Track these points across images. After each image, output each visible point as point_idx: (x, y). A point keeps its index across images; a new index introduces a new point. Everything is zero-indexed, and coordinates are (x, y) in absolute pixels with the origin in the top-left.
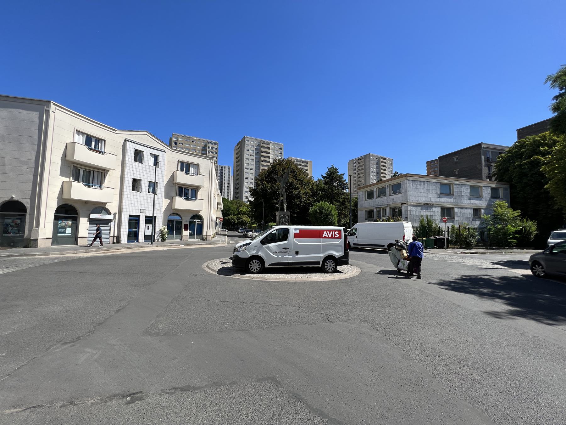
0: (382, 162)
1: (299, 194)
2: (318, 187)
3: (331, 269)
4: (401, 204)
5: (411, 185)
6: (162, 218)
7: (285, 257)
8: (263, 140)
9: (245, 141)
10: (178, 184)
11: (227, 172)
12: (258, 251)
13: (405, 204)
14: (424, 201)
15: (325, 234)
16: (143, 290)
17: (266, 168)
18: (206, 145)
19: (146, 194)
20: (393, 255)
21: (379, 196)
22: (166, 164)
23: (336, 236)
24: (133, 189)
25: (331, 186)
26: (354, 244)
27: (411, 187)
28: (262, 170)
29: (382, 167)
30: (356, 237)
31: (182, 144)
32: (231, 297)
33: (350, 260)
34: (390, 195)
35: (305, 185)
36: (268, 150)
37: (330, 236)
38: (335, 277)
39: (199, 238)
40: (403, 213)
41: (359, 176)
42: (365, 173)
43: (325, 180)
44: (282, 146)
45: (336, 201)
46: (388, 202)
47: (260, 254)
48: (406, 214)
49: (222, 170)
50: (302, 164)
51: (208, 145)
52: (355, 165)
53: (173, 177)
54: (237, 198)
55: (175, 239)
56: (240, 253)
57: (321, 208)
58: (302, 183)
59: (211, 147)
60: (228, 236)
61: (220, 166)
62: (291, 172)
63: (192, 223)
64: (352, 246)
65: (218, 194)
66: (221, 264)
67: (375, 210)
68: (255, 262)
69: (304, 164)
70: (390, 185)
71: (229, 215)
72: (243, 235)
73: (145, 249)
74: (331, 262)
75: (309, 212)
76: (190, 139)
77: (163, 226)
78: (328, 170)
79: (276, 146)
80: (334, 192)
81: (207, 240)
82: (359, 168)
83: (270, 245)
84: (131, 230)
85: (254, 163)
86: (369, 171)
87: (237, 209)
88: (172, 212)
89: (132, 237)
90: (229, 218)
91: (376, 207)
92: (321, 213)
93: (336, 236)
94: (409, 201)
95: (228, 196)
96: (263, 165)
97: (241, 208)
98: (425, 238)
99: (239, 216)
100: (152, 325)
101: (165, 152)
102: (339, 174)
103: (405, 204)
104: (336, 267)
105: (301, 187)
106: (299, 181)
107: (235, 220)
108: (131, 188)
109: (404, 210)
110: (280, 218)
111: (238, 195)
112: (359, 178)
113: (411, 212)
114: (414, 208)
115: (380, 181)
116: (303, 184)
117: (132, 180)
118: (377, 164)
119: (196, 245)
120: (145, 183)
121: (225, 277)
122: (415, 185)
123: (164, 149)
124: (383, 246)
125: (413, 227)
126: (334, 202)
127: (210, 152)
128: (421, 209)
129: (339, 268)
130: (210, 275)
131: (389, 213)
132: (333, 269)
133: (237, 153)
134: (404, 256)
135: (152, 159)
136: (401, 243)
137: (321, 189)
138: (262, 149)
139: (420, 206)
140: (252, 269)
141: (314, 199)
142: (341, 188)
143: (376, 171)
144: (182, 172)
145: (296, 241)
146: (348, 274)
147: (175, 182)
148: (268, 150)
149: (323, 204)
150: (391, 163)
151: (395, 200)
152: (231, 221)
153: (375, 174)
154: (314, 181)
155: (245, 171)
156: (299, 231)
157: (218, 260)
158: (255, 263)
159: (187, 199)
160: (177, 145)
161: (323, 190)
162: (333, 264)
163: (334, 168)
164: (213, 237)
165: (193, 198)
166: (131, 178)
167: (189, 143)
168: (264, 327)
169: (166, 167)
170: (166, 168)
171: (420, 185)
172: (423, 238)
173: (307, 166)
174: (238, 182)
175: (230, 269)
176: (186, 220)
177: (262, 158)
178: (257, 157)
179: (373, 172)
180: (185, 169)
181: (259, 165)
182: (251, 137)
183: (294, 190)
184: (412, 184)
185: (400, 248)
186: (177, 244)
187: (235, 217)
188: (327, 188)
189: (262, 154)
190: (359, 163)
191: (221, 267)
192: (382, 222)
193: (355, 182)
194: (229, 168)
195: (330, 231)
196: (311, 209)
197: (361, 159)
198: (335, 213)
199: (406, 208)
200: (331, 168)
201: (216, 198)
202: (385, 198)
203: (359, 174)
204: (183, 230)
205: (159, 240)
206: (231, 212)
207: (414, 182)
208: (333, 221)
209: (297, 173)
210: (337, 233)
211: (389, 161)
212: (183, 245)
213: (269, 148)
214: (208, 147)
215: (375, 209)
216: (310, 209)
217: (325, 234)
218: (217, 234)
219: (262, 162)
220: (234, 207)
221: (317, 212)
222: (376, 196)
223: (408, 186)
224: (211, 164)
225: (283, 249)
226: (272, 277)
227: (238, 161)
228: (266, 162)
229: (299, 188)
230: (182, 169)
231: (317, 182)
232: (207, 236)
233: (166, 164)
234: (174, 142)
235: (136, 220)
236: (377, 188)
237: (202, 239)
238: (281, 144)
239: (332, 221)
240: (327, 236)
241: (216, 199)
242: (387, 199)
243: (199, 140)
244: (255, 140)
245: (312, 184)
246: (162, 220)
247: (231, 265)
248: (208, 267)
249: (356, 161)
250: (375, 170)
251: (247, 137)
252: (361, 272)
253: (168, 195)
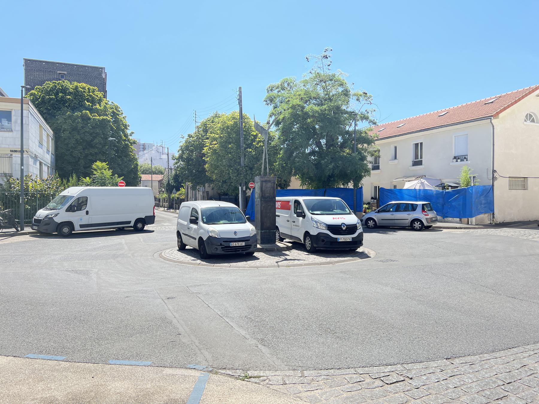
26: (81, 226)
30: (87, 213)
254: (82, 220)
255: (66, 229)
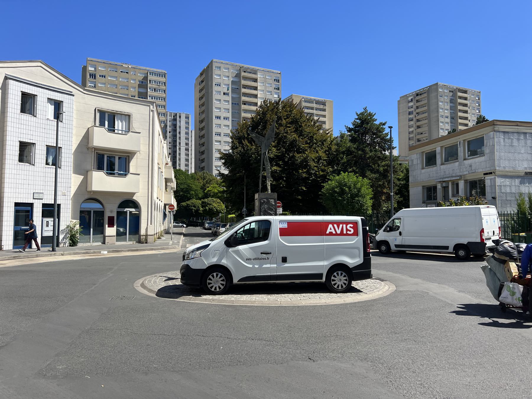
0: (460, 98)
1: (305, 160)
2: (340, 147)
3: (342, 287)
4: (485, 174)
5: (502, 141)
6: (70, 206)
7: (264, 266)
8: (246, 66)
9: (214, 68)
10: (96, 149)
11: (183, 124)
12: (221, 259)
13: (491, 173)
14: (526, 168)
15: (331, 229)
16: (37, 320)
17: (249, 115)
18: (146, 78)
19: (42, 167)
20: (492, 272)
21: (447, 160)
22: (75, 116)
23: (348, 232)
24: (21, 160)
25: (363, 144)
26: (396, 246)
27: (502, 143)
28: (245, 119)
29: (460, 107)
30: (400, 234)
31: (105, 77)
32: (170, 329)
33: (373, 271)
34: (465, 159)
35: (316, 144)
36: (253, 84)
37: (339, 232)
38: (346, 299)
39: (133, 239)
40: (488, 189)
41: (419, 124)
42: (428, 118)
43: (352, 135)
44: (279, 75)
45: (373, 171)
46: (462, 170)
47: (224, 262)
48: (494, 191)
49: (175, 120)
50: (314, 105)
51: (150, 77)
52: (411, 104)
53: (87, 137)
54: (203, 169)
55: (93, 242)
56: (192, 261)
57: (341, 185)
58: (311, 141)
59: (155, 81)
60: (185, 235)
61: (171, 113)
62: (291, 123)
63: (120, 214)
64: (393, 248)
65: (167, 164)
66: (166, 280)
67: (439, 186)
68: (217, 275)
69: (318, 106)
70: (464, 140)
71: (189, 199)
72: (212, 232)
73: (44, 259)
74: (342, 274)
75: (321, 192)
76: (118, 67)
77: (73, 220)
78: (357, 117)
79: (268, 76)
80: (368, 156)
81: (146, 243)
82: (418, 111)
83: (241, 247)
84: (18, 228)
85: (230, 107)
86: (436, 115)
87: (202, 188)
88: (87, 197)
89: (21, 239)
90: (188, 204)
91: (441, 180)
92: (342, 192)
93: (348, 232)
94: (497, 168)
95: (187, 165)
96: (246, 111)
97: (208, 187)
98: (523, 234)
99: (206, 200)
100: (48, 365)
101: (73, 95)
102: (377, 123)
103: (491, 173)
104: (350, 283)
105: (310, 147)
106: (305, 137)
107: (198, 207)
108: (17, 158)
109: (490, 185)
110: (261, 204)
111: (203, 165)
112: (419, 127)
113: (502, 187)
114: (507, 182)
115: (453, 132)
116: (313, 144)
117: (18, 144)
118: (451, 101)
119: (129, 251)
120: (41, 149)
121: (168, 301)
122: (510, 141)
123: (71, 91)
124: (447, 248)
125: (500, 215)
126: (368, 173)
127: (152, 90)
128: (520, 182)
129: (355, 284)
130: (143, 298)
131: (463, 190)
132: (344, 287)
133: (201, 91)
134: (511, 273)
135: (51, 109)
136: (506, 245)
137: (345, 151)
138: (243, 82)
139: (518, 177)
140: (212, 287)
141: (333, 167)
142: (381, 148)
143: (449, 115)
144: (102, 129)
145: (284, 241)
146: (370, 294)
147: (90, 145)
148: (253, 84)
149: (346, 177)
150: (477, 98)
151: (473, 168)
152: (193, 209)
153: (448, 120)
154: (334, 136)
155: (215, 121)
156: (286, 225)
157: (161, 274)
158: (217, 277)
159: (111, 174)
160: (95, 78)
161: (349, 152)
162: (345, 278)
163: (368, 112)
164: (159, 238)
165: (122, 172)
166: (17, 141)
167: (114, 74)
168: (211, 367)
169: (74, 120)
170: (74, 123)
171: (518, 140)
172: (521, 234)
173: (324, 110)
174: (203, 140)
175: (178, 289)
176: (111, 210)
177: (244, 98)
178: (234, 96)
179: (444, 117)
180: (107, 123)
181: (239, 110)
182: (224, 62)
183: (297, 153)
184: (504, 139)
185: (503, 258)
186: (97, 250)
187: (198, 202)
188: (355, 148)
189: (244, 90)
190: (418, 101)
191: (163, 284)
192: (449, 206)
193: (411, 136)
194: (187, 118)
195: (338, 223)
196: (327, 186)
197: (421, 94)
198: (367, 192)
199: (492, 181)
200: (362, 114)
201: (163, 170)
202: (457, 164)
203: (418, 120)
204: (107, 226)
205: (67, 244)
206: (192, 194)
207: (507, 134)
208: (364, 206)
209: (303, 125)
210: (350, 227)
211: (474, 95)
212: (106, 252)
213: (255, 80)
214: (150, 81)
215: (440, 185)
216: (323, 187)
217: (331, 229)
218: (167, 232)
219: (245, 104)
220: (196, 185)
221: (336, 192)
222: (440, 160)
223: (497, 143)
224: (151, 113)
225: (262, 253)
226: (242, 299)
227: (203, 105)
228: (251, 105)
229: (306, 150)
230: (102, 124)
231: (339, 139)
232: (146, 235)
233: (75, 116)
234: (90, 74)
235: (28, 211)
236: (442, 147)
237: (140, 242)
238: (277, 71)
239: (362, 206)
240: (334, 232)
241: (162, 172)
242: (460, 165)
243: (134, 68)
244: (230, 67)
245: (329, 143)
246: (70, 211)
247: (178, 282)
248: (143, 285)
249: (412, 97)
250: (447, 113)
251: (217, 60)
252: (396, 290)
253: (79, 169)
254: (397, 241)
255: (462, 252)
